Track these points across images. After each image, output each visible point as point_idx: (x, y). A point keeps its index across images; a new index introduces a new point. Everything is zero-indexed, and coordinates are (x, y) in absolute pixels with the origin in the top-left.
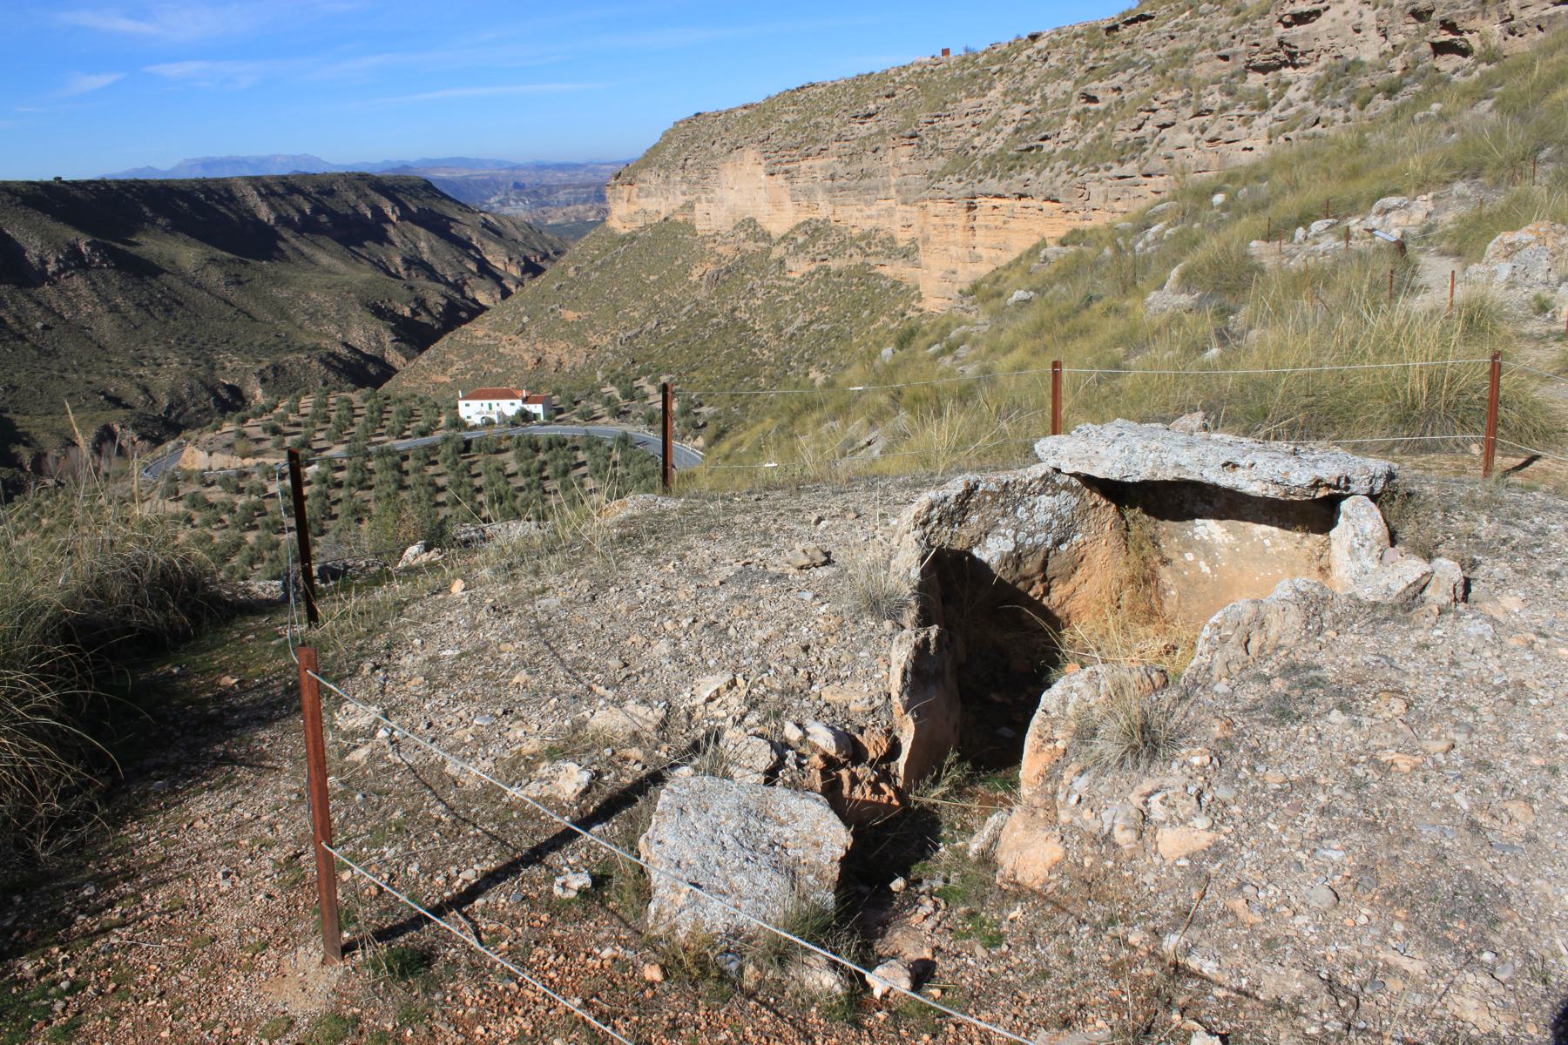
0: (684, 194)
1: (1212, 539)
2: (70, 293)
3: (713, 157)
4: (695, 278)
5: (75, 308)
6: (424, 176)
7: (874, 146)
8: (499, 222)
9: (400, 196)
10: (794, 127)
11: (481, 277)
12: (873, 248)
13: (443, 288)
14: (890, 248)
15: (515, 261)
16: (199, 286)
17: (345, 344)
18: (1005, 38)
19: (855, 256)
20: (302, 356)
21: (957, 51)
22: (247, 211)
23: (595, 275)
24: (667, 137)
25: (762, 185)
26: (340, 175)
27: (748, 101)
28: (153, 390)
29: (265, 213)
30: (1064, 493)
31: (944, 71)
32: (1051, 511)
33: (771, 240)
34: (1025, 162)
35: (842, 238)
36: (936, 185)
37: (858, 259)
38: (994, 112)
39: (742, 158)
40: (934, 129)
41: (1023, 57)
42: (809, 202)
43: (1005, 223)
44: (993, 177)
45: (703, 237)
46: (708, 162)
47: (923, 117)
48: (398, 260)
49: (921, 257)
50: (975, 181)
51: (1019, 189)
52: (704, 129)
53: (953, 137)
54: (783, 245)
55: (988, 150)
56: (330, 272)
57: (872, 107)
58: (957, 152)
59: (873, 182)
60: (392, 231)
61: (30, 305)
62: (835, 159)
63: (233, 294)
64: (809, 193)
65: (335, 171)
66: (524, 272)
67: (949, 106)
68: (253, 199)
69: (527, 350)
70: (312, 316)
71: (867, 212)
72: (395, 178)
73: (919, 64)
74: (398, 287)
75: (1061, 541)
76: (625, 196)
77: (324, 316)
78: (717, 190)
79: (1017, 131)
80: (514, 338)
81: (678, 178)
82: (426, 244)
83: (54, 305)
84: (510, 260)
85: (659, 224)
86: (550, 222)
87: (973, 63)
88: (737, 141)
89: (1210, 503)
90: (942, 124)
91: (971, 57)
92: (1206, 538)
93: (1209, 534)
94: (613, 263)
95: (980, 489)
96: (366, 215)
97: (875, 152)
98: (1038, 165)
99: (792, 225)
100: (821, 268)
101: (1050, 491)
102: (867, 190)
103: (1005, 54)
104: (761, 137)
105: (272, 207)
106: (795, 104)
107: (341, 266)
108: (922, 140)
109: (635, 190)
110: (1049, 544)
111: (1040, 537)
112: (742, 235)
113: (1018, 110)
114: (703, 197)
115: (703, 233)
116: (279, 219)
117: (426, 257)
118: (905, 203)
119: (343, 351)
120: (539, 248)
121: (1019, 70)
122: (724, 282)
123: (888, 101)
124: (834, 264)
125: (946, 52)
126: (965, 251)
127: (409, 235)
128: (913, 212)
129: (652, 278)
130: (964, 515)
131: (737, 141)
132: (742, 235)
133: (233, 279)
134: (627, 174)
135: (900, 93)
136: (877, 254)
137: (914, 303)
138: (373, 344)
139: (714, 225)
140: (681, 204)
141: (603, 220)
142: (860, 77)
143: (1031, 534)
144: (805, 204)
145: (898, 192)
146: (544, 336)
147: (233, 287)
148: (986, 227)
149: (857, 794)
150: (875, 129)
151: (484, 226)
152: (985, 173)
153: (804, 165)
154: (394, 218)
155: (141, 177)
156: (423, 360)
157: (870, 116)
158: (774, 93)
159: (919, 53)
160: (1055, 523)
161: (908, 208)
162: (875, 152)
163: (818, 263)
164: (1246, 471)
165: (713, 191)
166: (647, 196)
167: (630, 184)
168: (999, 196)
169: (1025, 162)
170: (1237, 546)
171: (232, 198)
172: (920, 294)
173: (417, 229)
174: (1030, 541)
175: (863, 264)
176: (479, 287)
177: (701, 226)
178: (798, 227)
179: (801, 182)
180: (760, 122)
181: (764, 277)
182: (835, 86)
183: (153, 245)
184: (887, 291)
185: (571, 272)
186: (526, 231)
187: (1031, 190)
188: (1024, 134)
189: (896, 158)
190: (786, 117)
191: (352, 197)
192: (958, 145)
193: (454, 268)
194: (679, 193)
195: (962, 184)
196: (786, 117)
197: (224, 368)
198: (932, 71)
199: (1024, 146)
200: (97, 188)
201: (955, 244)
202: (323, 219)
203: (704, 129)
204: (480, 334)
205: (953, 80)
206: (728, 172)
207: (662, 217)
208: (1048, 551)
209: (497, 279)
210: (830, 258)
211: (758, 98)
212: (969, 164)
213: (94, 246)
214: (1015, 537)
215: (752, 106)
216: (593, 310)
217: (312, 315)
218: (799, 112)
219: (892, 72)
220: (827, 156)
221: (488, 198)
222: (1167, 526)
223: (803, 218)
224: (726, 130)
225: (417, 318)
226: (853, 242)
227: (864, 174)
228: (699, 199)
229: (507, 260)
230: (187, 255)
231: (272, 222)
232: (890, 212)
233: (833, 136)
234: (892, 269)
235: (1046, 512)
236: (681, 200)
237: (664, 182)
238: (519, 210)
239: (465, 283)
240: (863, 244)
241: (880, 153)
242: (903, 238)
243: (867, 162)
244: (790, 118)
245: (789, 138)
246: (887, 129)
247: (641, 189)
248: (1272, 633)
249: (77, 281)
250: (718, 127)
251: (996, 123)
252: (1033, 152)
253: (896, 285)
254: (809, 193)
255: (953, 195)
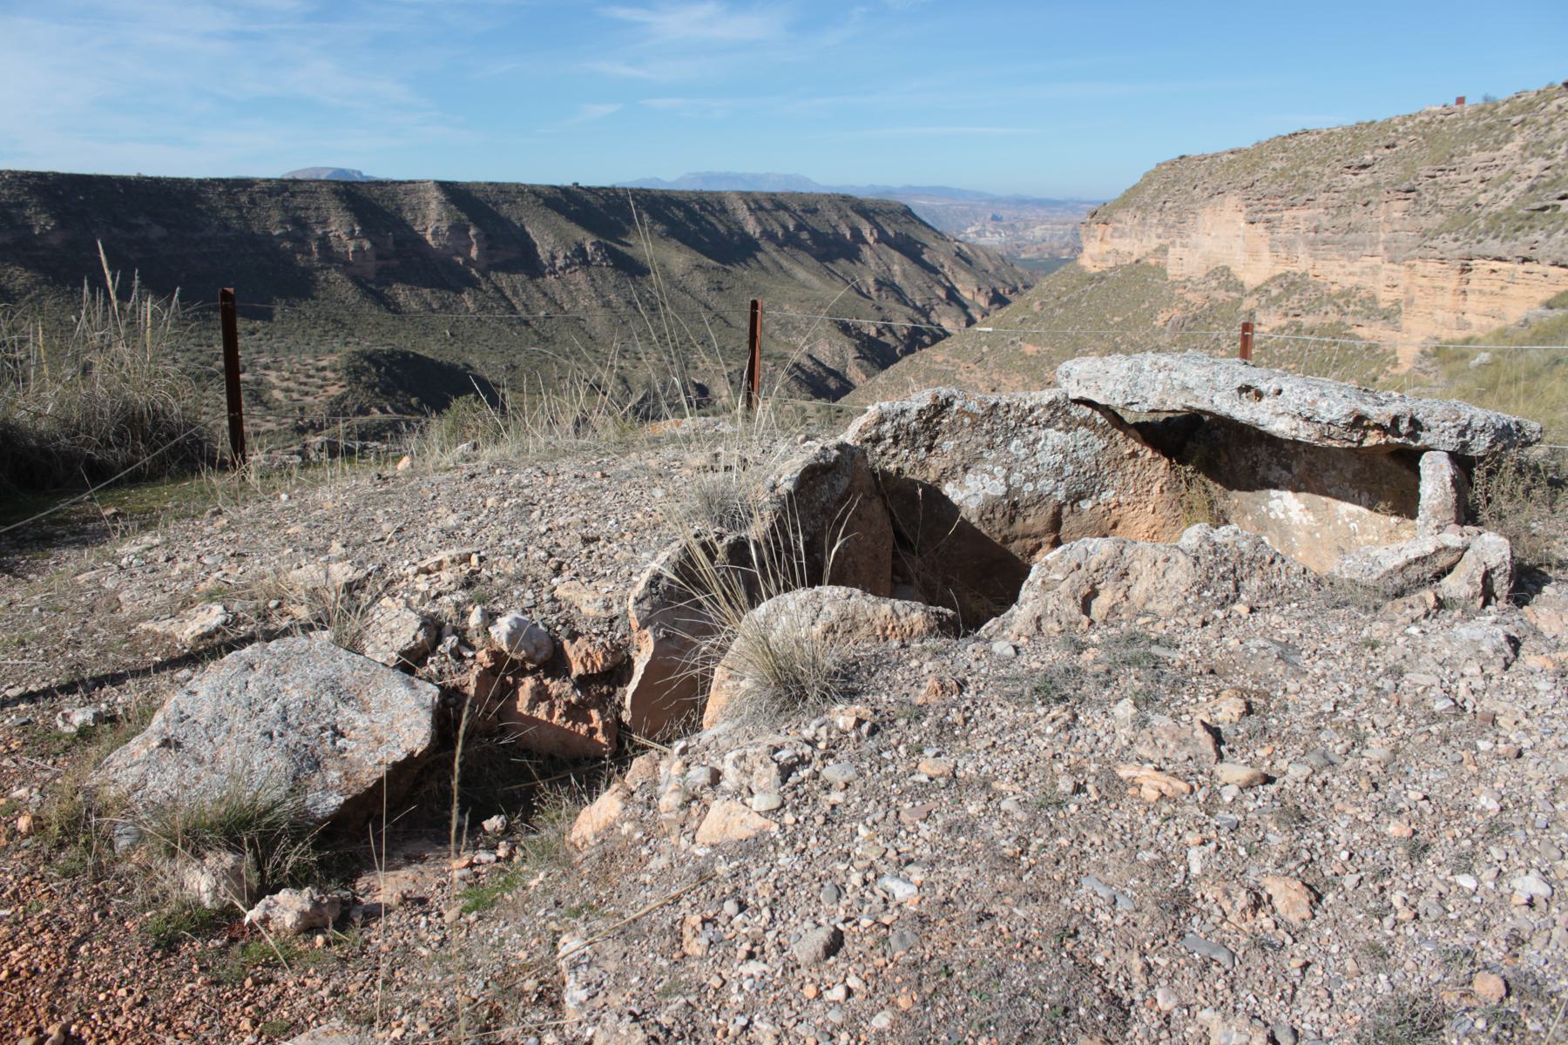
0: (1159, 237)
1: (1289, 519)
2: (572, 287)
3: (1193, 201)
4: (1159, 323)
5: (574, 301)
6: (905, 203)
7: (1366, 200)
8: (972, 251)
9: (879, 219)
10: (1281, 175)
11: (948, 304)
12: (1352, 307)
13: (911, 311)
14: (1372, 309)
15: (984, 291)
16: (684, 290)
17: (810, 356)
18: (1534, 85)
19: (1331, 314)
20: (769, 364)
21: (1474, 99)
22: (736, 224)
23: (1059, 311)
24: (1149, 178)
25: (1240, 233)
26: (825, 195)
27: (1235, 146)
28: (630, 381)
29: (752, 227)
30: (1082, 430)
31: (1456, 121)
32: (1062, 451)
33: (1243, 291)
34: (1536, 223)
35: (1319, 294)
36: (1428, 244)
37: (1334, 317)
38: (1508, 167)
39: (1222, 204)
40: (1435, 183)
41: (1553, 107)
42: (1288, 254)
43: (1502, 288)
44: (1495, 237)
45: (1173, 282)
46: (1187, 206)
47: (1425, 170)
48: (870, 281)
49: (1406, 322)
50: (1474, 241)
51: (1524, 251)
52: (1187, 173)
53: (1456, 193)
54: (1256, 296)
55: (1493, 209)
56: (805, 287)
57: (1368, 158)
58: (1458, 209)
59: (1361, 237)
60: (866, 252)
61: (538, 295)
62: (1322, 210)
63: (714, 299)
64: (1289, 245)
65: (815, 190)
66: (991, 303)
67: (1455, 159)
68: (743, 213)
69: (983, 380)
70: (783, 326)
71: (1350, 268)
72: (877, 202)
73: (1428, 113)
74: (867, 305)
75: (1080, 496)
76: (1099, 234)
77: (794, 328)
78: (1193, 235)
79: (1532, 188)
80: (972, 366)
81: (1155, 221)
82: (899, 267)
83: (557, 297)
84: (979, 290)
85: (1130, 266)
86: (1023, 256)
87: (1491, 113)
88: (1219, 186)
89: (1288, 468)
90: (1445, 178)
91: (1489, 107)
92: (1282, 516)
93: (1285, 511)
94: (1079, 301)
95: (956, 407)
96: (844, 236)
97: (1365, 205)
98: (1550, 227)
99: (1267, 277)
100: (1293, 323)
101: (1061, 425)
102: (1352, 245)
103: (1530, 104)
104: (1245, 184)
105: (759, 221)
106: (1285, 151)
107: (815, 282)
108: (1420, 195)
109: (1109, 229)
110: (1060, 495)
111: (1046, 485)
112: (1214, 283)
113: (1536, 166)
114: (1178, 241)
115: (1174, 278)
116: (764, 232)
117: (898, 280)
118: (1392, 261)
119: (807, 363)
120: (1009, 280)
121: (1546, 121)
122: (1189, 329)
123: (1387, 151)
124: (1307, 321)
125: (1460, 101)
126: (1453, 316)
127: (884, 257)
128: (1400, 273)
129: (1116, 319)
130: (933, 438)
131: (1219, 186)
132: (1214, 283)
133: (715, 286)
134: (1101, 214)
135: (1402, 144)
136: (1355, 313)
137: (1388, 368)
138: (837, 359)
139: (1186, 271)
140: (1155, 247)
141: (1076, 259)
142: (1359, 126)
143: (1031, 478)
144: (1284, 255)
145: (1386, 249)
146: (1001, 366)
147: (714, 293)
148: (1480, 292)
149: (541, 713)
150: (1369, 181)
151: (957, 254)
152: (1487, 233)
153: (1287, 215)
154: (871, 240)
155: (645, 187)
156: (881, 377)
157: (1365, 167)
158: (1264, 138)
159: (1433, 101)
160: (1069, 469)
161: (1395, 267)
162: (1365, 205)
163: (1290, 319)
164: (1272, 401)
165: (1188, 236)
166: (1121, 237)
167: (1105, 223)
168: (1500, 259)
169: (1536, 223)
170: (1318, 529)
171: (724, 211)
172: (1396, 359)
173: (892, 251)
174: (1029, 487)
175: (1339, 323)
176: (944, 313)
177: (1173, 271)
178: (1273, 279)
179: (1282, 233)
180: (1245, 167)
181: (1231, 328)
182: (1331, 134)
183: (646, 245)
184: (1361, 353)
185: (1036, 307)
186: (998, 262)
187: (1538, 254)
188: (1540, 192)
189: (1387, 212)
190: (1274, 164)
191: (834, 217)
192: (1461, 202)
193: (924, 293)
194: (1153, 236)
195: (1459, 243)
196: (1274, 164)
197: (696, 368)
198: (1442, 121)
199: (1537, 205)
200: (607, 194)
201: (1442, 308)
202: (804, 235)
203: (1187, 173)
204: (939, 359)
205: (1465, 131)
206: (1206, 218)
207: (1134, 259)
208: (1060, 506)
209: (964, 307)
210: (1303, 314)
211: (1247, 143)
212: (1470, 221)
213: (598, 246)
214: (1007, 478)
215: (1240, 151)
216: (1053, 346)
217: (783, 326)
218: (1289, 159)
219: (1396, 121)
220: (1313, 207)
221: (966, 228)
222: (1237, 497)
223: (1280, 270)
224: (1210, 174)
225: (881, 339)
226: (1331, 299)
227: (1351, 229)
228: (1173, 243)
229: (975, 290)
230: (679, 259)
231: (757, 235)
232: (1375, 270)
233: (1322, 186)
234: (1369, 332)
235: (1054, 452)
236: (1155, 243)
237: (1140, 224)
238: (993, 240)
239: (932, 309)
240: (1341, 302)
241: (1372, 207)
242: (1385, 298)
243: (1356, 216)
244: (1278, 165)
245: (1274, 186)
246: (1383, 182)
247: (1115, 229)
248: (1137, 592)
249: (580, 277)
250: (1201, 171)
251: (1507, 180)
252: (1547, 212)
253: (1371, 348)
254: (1289, 245)
255: (1447, 255)
